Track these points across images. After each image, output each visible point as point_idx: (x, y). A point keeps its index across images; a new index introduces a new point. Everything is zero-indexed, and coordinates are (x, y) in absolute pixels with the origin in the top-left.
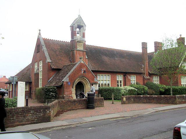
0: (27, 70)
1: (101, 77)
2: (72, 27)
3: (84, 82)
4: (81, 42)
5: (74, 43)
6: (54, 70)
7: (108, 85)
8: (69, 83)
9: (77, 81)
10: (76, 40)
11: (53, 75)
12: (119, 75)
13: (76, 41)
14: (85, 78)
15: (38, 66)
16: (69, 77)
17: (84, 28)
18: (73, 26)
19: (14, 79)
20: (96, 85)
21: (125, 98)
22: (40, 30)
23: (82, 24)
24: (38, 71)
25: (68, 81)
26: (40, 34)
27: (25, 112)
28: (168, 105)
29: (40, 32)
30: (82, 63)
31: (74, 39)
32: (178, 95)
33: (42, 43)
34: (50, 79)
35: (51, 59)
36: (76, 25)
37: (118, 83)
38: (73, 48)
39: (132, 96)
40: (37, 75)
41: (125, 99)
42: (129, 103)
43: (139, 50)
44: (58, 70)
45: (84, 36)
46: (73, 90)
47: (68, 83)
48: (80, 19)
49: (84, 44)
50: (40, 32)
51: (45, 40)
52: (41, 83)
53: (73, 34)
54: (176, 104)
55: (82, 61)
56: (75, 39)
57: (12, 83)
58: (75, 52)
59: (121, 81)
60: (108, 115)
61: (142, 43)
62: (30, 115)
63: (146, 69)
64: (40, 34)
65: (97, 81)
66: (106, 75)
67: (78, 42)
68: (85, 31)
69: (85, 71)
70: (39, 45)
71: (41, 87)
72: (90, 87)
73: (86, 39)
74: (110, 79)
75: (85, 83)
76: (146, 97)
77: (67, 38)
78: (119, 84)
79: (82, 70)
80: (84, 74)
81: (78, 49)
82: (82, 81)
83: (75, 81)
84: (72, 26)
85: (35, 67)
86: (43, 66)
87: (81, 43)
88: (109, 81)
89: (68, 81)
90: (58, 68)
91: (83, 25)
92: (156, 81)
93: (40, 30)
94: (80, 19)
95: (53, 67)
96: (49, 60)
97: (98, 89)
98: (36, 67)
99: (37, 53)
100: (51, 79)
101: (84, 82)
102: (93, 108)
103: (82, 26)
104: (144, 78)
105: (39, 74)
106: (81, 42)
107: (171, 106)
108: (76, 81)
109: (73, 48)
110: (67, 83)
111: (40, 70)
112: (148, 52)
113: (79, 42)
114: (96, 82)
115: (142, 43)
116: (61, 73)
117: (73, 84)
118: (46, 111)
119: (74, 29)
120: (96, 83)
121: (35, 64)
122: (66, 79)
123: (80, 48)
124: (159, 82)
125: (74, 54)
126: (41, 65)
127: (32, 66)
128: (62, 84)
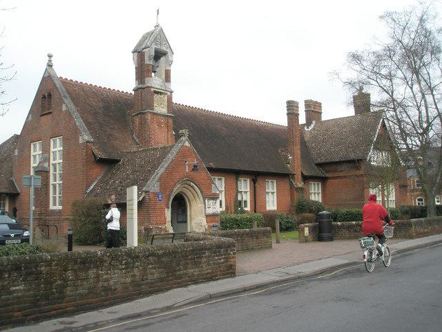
2: (139, 53)
4: (161, 93)
5: (144, 94)
9: (176, 191)
10: (151, 87)
11: (98, 173)
12: (217, 178)
13: (152, 89)
15: (46, 150)
16: (160, 179)
19: (33, 184)
22: (50, 56)
23: (165, 49)
24: (46, 165)
26: (50, 66)
28: (400, 240)
29: (50, 61)
34: (92, 187)
35: (91, 134)
40: (43, 173)
41: (308, 232)
45: (168, 78)
47: (158, 197)
48: (157, 36)
50: (50, 61)
52: (57, 195)
53: (142, 72)
54: (411, 237)
58: (149, 117)
63: (295, 162)
64: (50, 66)
65: (218, 192)
67: (155, 92)
69: (195, 166)
70: (50, 95)
71: (275, 208)
72: (203, 205)
73: (173, 86)
74: (275, 191)
75: (191, 196)
76: (350, 227)
77: (123, 81)
80: (195, 174)
82: (185, 191)
83: (172, 191)
86: (66, 154)
87: (162, 96)
88: (246, 192)
92: (315, 194)
93: (50, 56)
94: (157, 36)
95: (100, 155)
96: (85, 137)
98: (36, 151)
99: (42, 115)
101: (189, 194)
103: (165, 54)
106: (161, 93)
107: (402, 243)
110: (156, 194)
111: (52, 162)
112: (287, 125)
114: (215, 194)
115: (321, 104)
121: (32, 146)
123: (161, 108)
124: (320, 195)
125: (145, 123)
126: (57, 147)
127: (21, 151)
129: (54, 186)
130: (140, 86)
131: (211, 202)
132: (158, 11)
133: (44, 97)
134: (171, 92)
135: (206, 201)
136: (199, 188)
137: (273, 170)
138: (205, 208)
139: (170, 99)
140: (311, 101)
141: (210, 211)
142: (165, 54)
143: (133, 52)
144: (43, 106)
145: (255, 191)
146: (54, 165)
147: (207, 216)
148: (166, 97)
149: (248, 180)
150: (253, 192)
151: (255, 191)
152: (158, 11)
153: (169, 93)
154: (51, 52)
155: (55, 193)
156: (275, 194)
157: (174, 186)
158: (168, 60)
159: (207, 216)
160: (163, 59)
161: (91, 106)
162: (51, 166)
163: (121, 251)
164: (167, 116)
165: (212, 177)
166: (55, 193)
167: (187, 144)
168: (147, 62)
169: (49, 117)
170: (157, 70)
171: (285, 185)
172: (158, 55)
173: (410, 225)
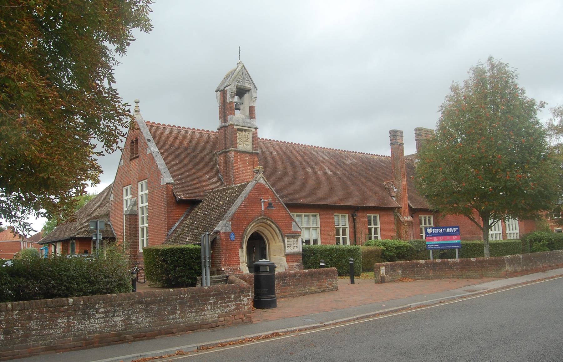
0: (100, 207)
1: (304, 219)
3: (266, 233)
4: (245, 131)
6: (182, 203)
7: (315, 242)
8: (232, 236)
9: (250, 230)
10: (234, 125)
13: (235, 127)
14: (269, 222)
15: (135, 193)
16: (232, 219)
17: (254, 95)
18: (227, 88)
19: (98, 228)
20: (296, 239)
21: (384, 268)
22: (131, 105)
23: (247, 85)
24: (135, 208)
25: (229, 229)
27: (198, 301)
30: (261, 184)
31: (228, 124)
32: (508, 256)
33: (146, 134)
35: (173, 176)
36: (231, 89)
37: (338, 234)
38: (226, 145)
39: (398, 264)
40: (133, 218)
42: (392, 281)
43: (386, 152)
44: (192, 204)
45: (252, 114)
46: (243, 255)
49: (255, 137)
51: (152, 126)
52: (145, 238)
55: (261, 179)
56: (231, 123)
57: (94, 238)
58: (232, 155)
59: (344, 231)
60: (559, 275)
61: (391, 132)
62: (209, 307)
65: (299, 230)
66: (308, 216)
67: (238, 129)
68: (254, 101)
69: (270, 204)
70: (137, 140)
74: (319, 226)
75: (269, 235)
78: (341, 236)
79: (262, 200)
81: (240, 147)
82: (262, 229)
83: (245, 231)
84: (222, 88)
85: (125, 198)
86: (150, 198)
87: (247, 133)
88: (315, 229)
89: (229, 229)
90: (192, 198)
91: (251, 87)
93: (131, 105)
95: (181, 196)
96: (167, 179)
97: (301, 250)
98: (127, 197)
99: (131, 160)
100: (176, 225)
101: (266, 232)
102: (271, 304)
103: (248, 90)
104: (398, 219)
105: (137, 215)
106: (245, 131)
108: (248, 231)
109: (228, 145)
110: (227, 234)
111: (140, 205)
113: (241, 130)
114: (296, 232)
115: (391, 132)
116: (199, 211)
117: (242, 239)
118: (242, 298)
119: (228, 96)
120: (295, 235)
122: (222, 226)
126: (143, 192)
127: (116, 196)
128: (215, 239)
129: (143, 229)
130: (223, 124)
131: (292, 240)
132: (239, 48)
133: (132, 142)
134: (256, 129)
135: (286, 240)
136: (277, 226)
137: (339, 203)
138: (285, 247)
139: (255, 136)
140: (421, 129)
141: (288, 250)
142: (248, 90)
143: (216, 91)
144: (132, 151)
145: (355, 228)
146: (142, 208)
147: (287, 255)
148: (250, 136)
149: (347, 215)
150: (352, 231)
151: (355, 228)
152: (239, 48)
153: (254, 130)
154: (137, 99)
155: (143, 236)
156: (319, 230)
157: (248, 225)
158: (251, 97)
159: (287, 255)
160: (246, 96)
161: (177, 149)
162: (139, 209)
163: (20, 280)
164: (252, 153)
165: (291, 214)
166: (143, 236)
167: (262, 181)
168: (229, 99)
169: (136, 161)
170: (241, 107)
171: (390, 218)
172: (241, 92)
173: (503, 262)
